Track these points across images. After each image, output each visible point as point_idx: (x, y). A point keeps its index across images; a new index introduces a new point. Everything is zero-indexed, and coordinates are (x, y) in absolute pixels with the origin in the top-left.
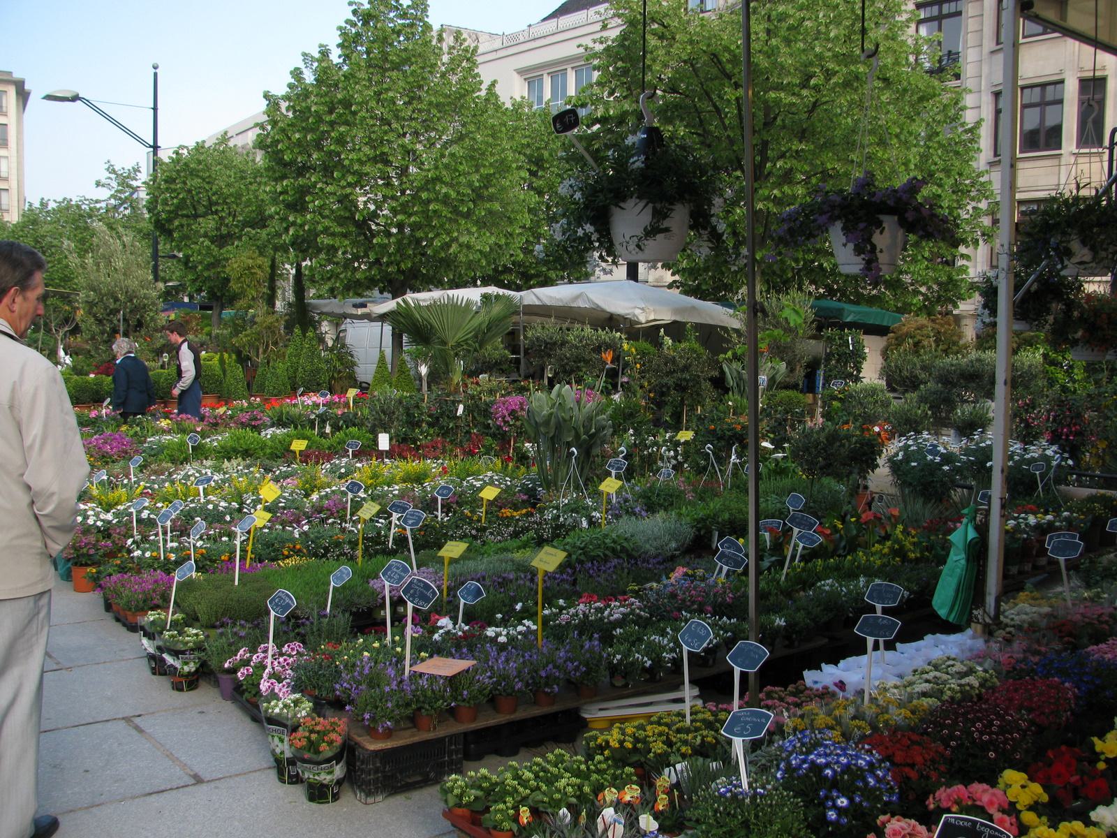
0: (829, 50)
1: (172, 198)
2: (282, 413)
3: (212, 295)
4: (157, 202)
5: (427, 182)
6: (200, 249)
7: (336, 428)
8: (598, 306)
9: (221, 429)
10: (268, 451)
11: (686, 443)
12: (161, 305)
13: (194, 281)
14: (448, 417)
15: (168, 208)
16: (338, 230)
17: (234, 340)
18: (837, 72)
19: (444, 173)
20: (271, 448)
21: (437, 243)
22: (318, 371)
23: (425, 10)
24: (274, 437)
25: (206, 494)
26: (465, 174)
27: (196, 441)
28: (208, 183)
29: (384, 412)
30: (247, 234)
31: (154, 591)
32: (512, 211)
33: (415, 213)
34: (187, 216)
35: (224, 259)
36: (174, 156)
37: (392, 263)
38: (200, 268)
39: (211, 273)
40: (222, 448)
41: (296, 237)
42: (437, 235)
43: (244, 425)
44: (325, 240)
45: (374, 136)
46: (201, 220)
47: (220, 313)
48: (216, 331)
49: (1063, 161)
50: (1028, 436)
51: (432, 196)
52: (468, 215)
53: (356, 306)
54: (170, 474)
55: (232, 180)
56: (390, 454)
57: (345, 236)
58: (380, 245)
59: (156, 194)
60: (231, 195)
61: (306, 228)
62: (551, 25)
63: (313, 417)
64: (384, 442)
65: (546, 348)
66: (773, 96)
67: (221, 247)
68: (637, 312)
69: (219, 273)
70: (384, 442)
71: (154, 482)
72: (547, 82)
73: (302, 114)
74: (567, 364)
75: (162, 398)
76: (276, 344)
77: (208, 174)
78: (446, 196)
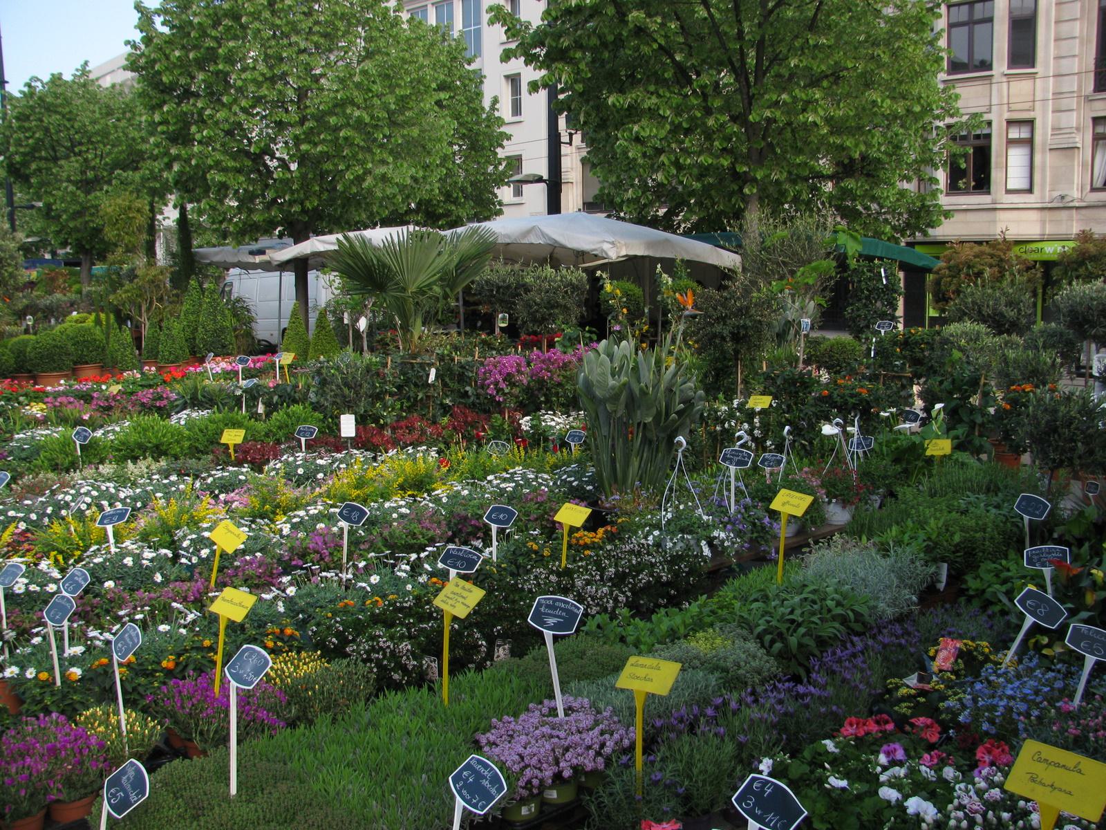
1: (28, 138)
2: (196, 388)
3: (80, 248)
4: (8, 143)
5: (336, 106)
6: (64, 195)
7: (271, 408)
9: (116, 414)
10: (186, 444)
11: (763, 412)
12: (21, 259)
13: (58, 233)
14: (416, 385)
15: (22, 150)
16: (231, 164)
17: (111, 298)
19: (356, 93)
20: (189, 439)
21: (349, 176)
22: (223, 330)
24: (190, 424)
25: (118, 538)
26: (379, 96)
27: (85, 438)
28: (69, 120)
29: (346, 384)
30: (118, 177)
31: (50, 774)
32: (430, 139)
34: (46, 159)
35: (93, 206)
36: (26, 89)
37: (295, 201)
38: (64, 217)
39: (77, 223)
40: (123, 444)
41: (181, 173)
42: (348, 167)
43: (146, 409)
44: (215, 176)
45: (270, 52)
46: (62, 162)
47: (90, 270)
48: (86, 289)
49: (994, 80)
50: (1007, 380)
51: (342, 121)
53: (252, 253)
54: (53, 493)
55: (97, 115)
57: (239, 171)
59: (8, 133)
60: (97, 133)
61: (193, 162)
63: (239, 393)
64: (348, 426)
65: (507, 295)
67: (88, 193)
68: (606, 246)
69: (87, 222)
70: (348, 426)
71: (30, 510)
73: (182, 29)
74: (537, 311)
75: (30, 372)
76: (160, 300)
77: (67, 110)
78: (359, 120)
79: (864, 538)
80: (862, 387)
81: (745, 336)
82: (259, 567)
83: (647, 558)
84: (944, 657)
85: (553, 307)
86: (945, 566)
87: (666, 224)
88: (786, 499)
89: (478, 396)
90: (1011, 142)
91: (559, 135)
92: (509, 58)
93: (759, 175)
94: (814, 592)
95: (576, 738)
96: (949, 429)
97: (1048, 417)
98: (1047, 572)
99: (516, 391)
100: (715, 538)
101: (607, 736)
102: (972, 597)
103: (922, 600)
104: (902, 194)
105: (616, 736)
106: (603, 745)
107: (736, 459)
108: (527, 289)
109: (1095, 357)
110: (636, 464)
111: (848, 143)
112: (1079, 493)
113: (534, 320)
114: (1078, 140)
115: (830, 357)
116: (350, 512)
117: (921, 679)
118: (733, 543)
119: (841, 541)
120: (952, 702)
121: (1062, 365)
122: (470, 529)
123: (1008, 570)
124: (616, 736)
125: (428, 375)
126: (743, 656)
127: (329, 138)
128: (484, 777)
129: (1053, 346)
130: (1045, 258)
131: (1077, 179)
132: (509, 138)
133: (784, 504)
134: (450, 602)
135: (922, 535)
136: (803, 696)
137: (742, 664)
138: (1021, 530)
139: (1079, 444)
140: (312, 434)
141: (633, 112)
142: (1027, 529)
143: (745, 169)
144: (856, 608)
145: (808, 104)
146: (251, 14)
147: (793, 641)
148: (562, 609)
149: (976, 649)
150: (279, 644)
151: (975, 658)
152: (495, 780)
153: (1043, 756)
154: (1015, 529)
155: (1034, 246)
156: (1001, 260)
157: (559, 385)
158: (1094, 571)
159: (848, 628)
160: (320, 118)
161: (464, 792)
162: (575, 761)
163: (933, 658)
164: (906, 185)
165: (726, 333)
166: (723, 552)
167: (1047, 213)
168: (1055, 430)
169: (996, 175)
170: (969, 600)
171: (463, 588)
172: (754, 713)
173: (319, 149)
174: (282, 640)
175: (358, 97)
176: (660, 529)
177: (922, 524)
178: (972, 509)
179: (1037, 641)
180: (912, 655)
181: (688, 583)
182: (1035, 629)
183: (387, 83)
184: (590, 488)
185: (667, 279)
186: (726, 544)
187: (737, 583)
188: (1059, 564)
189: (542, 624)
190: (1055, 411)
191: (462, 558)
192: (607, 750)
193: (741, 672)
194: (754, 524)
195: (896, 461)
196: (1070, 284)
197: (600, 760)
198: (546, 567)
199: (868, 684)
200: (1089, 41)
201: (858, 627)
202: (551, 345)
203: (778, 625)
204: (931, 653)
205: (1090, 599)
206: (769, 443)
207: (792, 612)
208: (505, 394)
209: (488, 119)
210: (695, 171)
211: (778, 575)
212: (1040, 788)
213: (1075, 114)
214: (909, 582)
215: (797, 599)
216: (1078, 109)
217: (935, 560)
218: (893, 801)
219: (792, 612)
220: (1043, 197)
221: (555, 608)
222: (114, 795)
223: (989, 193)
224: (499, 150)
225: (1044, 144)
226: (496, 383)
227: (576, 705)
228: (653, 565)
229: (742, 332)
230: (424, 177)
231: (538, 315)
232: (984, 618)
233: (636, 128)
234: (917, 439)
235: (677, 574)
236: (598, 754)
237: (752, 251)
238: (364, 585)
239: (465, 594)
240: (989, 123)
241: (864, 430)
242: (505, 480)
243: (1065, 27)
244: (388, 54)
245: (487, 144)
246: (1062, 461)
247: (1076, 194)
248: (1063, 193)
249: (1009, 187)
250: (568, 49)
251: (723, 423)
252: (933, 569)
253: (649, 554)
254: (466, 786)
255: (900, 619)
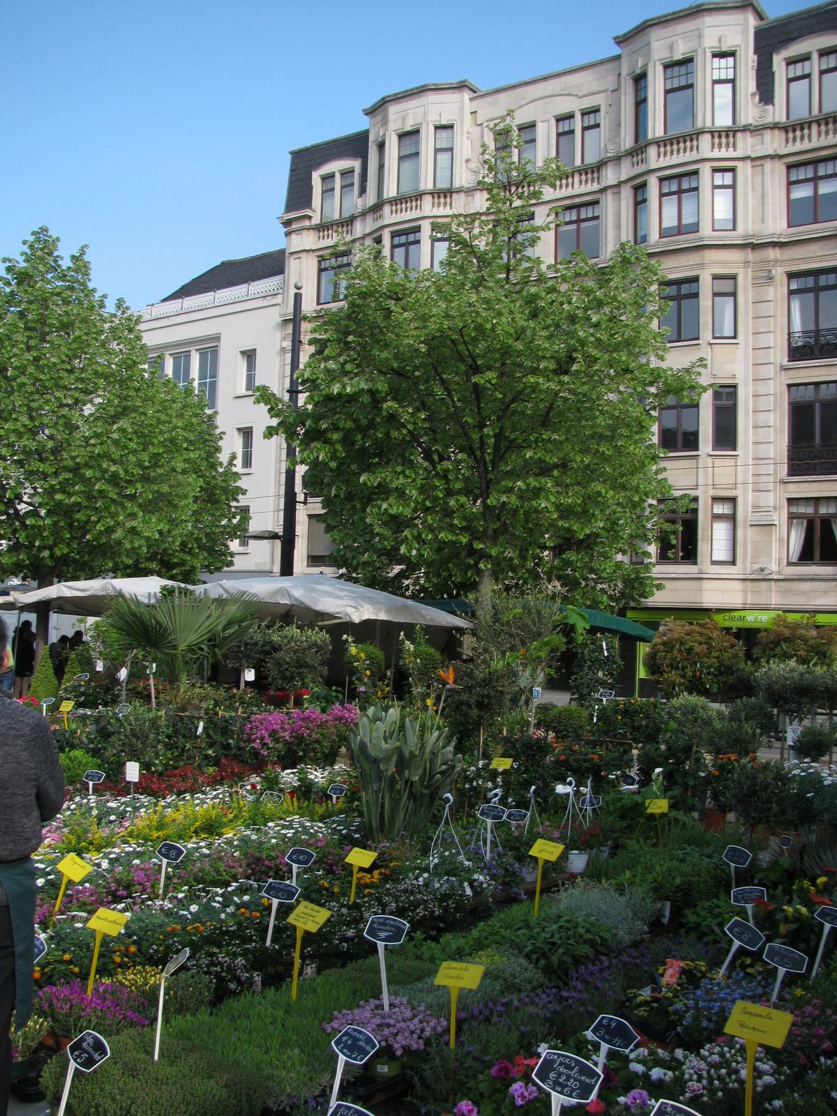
0: (592, 335)
8: (302, 603)
11: (505, 772)
14: (184, 736)
18: (598, 359)
19: (113, 449)
21: (100, 527)
23: (86, 274)
26: (134, 452)
29: (134, 735)
33: (76, 493)
49: (700, 461)
51: (98, 474)
52: (132, 498)
56: (141, 788)
58: (33, 527)
62: (175, 305)
64: (132, 772)
66: (532, 380)
68: (350, 610)
70: (132, 772)
72: (195, 360)
78: (115, 475)
79: (604, 880)
80: (593, 753)
81: (489, 704)
82: (92, 895)
83: (419, 896)
84: (670, 975)
85: (301, 666)
86: (669, 903)
87: (393, 586)
88: (542, 847)
89: (240, 748)
90: (717, 517)
91: (295, 494)
92: (272, 436)
93: (493, 552)
94: (568, 921)
95: (403, 1025)
96: (665, 790)
97: (749, 783)
98: (749, 907)
99: (280, 746)
100: (475, 880)
101: (425, 1024)
102: (691, 929)
103: (650, 932)
104: (619, 565)
105: (432, 1024)
106: (423, 1030)
107: (492, 813)
108: (276, 648)
109: (789, 729)
110: (402, 816)
111: (575, 527)
112: (776, 848)
113: (284, 678)
114: (775, 518)
115: (559, 722)
116: (168, 850)
117: (653, 990)
118: (489, 885)
119: (583, 883)
120: (678, 1006)
121: (761, 735)
122: (263, 869)
123: (719, 907)
124: (432, 1024)
125: (197, 728)
126: (518, 969)
127: (83, 489)
128: (361, 1040)
129: (753, 718)
130: (747, 625)
131: (775, 555)
132: (244, 492)
133: (540, 851)
134: (302, 920)
135: (649, 878)
136: (566, 999)
137: (517, 974)
138: (729, 875)
139: (774, 805)
140: (99, 778)
141: (383, 491)
142: (733, 874)
143: (481, 546)
144: (601, 934)
145: (537, 492)
146: (16, 368)
147: (555, 958)
148: (392, 926)
149: (695, 968)
150: (126, 959)
151: (695, 976)
152: (369, 1041)
153: (748, 1010)
154: (723, 875)
155: (737, 614)
156: (710, 638)
157: (317, 741)
158: (785, 907)
159: (596, 950)
160: (76, 470)
161: (345, 1050)
162: (404, 1042)
163: (662, 975)
164: (619, 557)
165: (472, 701)
166: (481, 892)
167: (749, 583)
168: (755, 793)
169: (702, 547)
170: (688, 932)
171: (312, 909)
172: (531, 1009)
173: (73, 499)
174: (127, 957)
175: (116, 453)
176: (429, 872)
177: (649, 869)
178: (688, 859)
179: (742, 963)
180: (646, 972)
181: (455, 918)
182: (741, 952)
183: (142, 440)
184: (357, 836)
185: (409, 645)
186: (485, 885)
187: (502, 915)
188: (758, 901)
189: (375, 937)
190: (755, 778)
191: (283, 890)
192: (427, 1033)
193: (517, 981)
194: (507, 870)
195: (622, 817)
196: (768, 662)
197: (421, 1042)
198: (338, 902)
199: (615, 992)
200: (782, 431)
201: (603, 950)
202: (298, 703)
203: (542, 946)
204: (661, 971)
205: (783, 929)
206: (510, 800)
207: (552, 936)
208: (269, 748)
209: (225, 474)
210: (435, 546)
211: (536, 909)
212: (746, 1030)
213: (772, 494)
214: (641, 915)
215: (555, 927)
216: (775, 490)
217: (661, 898)
218: (640, 1072)
219: (552, 936)
220: (745, 569)
221: (386, 925)
222: (79, 1056)
223: (695, 563)
224: (233, 504)
225: (745, 520)
226: (262, 738)
227: (397, 1002)
228: (426, 901)
229: (486, 701)
230: (169, 531)
231: (288, 673)
232: (701, 945)
233: (384, 506)
234: (638, 798)
235: (446, 909)
236: (420, 1037)
237: (486, 622)
238: (185, 913)
239: (314, 914)
240: (696, 499)
241: (596, 790)
242: (284, 827)
243: (761, 416)
244: (145, 414)
245: (223, 497)
246: (760, 819)
247: (774, 568)
248: (762, 566)
249: (714, 558)
250: (325, 431)
251: (471, 781)
252: (659, 905)
253: (420, 893)
254: (346, 1046)
255: (635, 945)
